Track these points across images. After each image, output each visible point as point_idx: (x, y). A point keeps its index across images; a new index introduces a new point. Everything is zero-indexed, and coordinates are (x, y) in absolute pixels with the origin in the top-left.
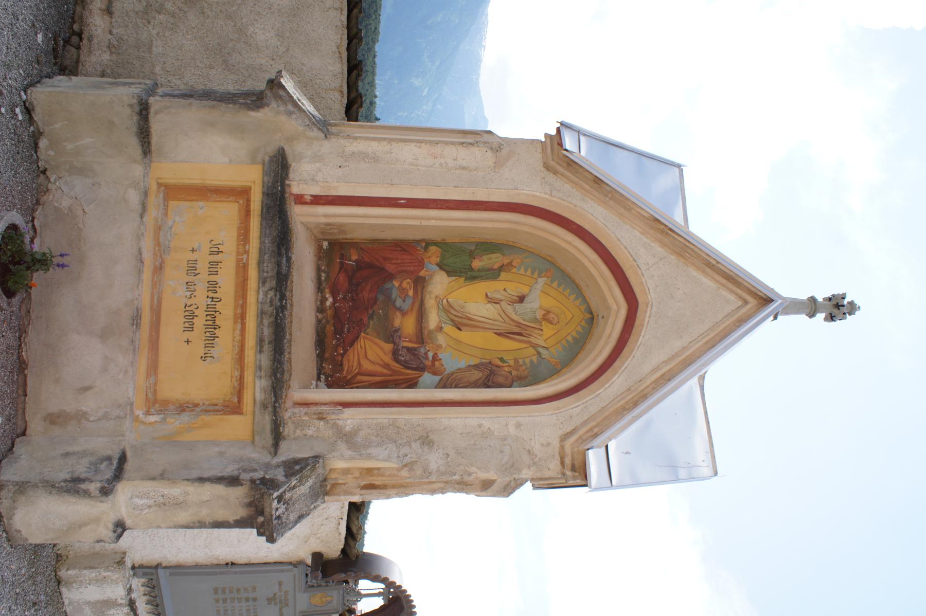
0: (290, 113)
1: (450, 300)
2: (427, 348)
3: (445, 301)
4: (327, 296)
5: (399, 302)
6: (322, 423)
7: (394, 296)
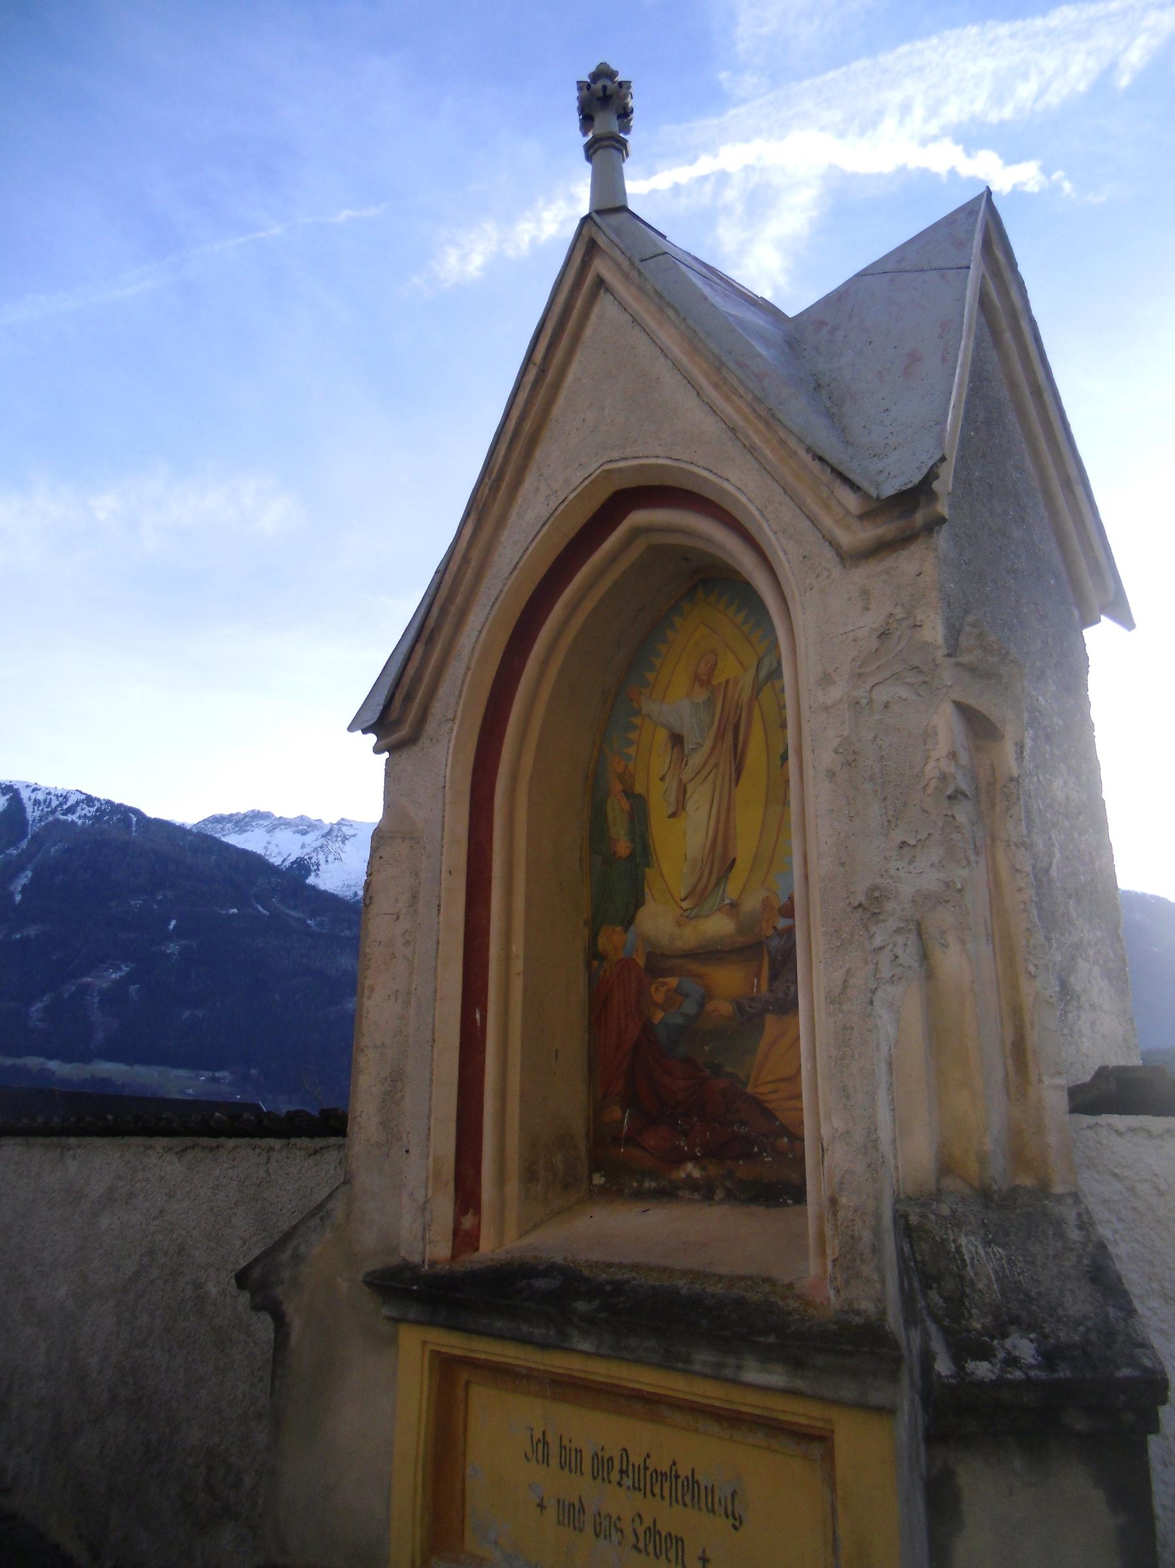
0: (297, 1258)
1: (683, 894)
2: (770, 932)
3: (685, 905)
4: (683, 1175)
5: (690, 1008)
6: (843, 1200)
7: (679, 1020)
